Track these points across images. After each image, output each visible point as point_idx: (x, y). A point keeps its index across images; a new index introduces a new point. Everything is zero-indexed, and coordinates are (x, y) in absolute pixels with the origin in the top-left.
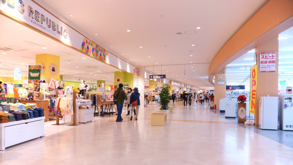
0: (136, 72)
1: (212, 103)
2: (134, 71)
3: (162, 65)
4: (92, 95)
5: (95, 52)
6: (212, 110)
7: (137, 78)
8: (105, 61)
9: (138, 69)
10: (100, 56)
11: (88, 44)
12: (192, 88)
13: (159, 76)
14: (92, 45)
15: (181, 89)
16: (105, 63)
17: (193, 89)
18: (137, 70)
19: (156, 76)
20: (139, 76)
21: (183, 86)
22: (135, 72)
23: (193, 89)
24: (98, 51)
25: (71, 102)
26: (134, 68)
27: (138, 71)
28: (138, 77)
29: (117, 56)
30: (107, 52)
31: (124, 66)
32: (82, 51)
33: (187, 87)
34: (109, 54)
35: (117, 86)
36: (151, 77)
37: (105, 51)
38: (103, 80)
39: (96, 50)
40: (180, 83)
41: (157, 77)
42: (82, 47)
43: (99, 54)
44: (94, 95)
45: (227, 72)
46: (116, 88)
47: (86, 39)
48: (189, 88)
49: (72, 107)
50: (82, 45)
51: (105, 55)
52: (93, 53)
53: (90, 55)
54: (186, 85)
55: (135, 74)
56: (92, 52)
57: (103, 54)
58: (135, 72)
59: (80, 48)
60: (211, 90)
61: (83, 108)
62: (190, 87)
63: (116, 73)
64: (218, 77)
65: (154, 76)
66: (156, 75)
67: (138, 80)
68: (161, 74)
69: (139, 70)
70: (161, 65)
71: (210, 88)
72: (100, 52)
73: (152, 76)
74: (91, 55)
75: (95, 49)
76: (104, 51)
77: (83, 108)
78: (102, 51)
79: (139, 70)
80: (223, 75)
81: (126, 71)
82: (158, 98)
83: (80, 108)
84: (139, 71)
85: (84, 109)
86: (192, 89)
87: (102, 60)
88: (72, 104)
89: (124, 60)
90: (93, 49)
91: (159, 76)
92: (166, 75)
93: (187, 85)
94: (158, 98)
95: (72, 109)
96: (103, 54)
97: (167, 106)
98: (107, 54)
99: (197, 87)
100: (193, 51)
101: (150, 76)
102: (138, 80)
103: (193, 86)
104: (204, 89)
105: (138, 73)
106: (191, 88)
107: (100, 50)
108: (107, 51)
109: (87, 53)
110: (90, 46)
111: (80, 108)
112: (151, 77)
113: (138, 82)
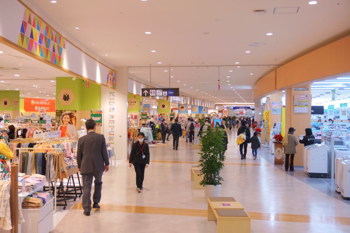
0: (110, 80)
1: (279, 151)
2: (108, 79)
3: (171, 65)
4: (36, 155)
5: (43, 45)
6: (276, 165)
7: (110, 93)
8: (60, 66)
9: (114, 72)
10: (52, 51)
11: (32, 26)
12: (203, 106)
13: (164, 90)
14: (38, 29)
15: (182, 108)
16: (60, 68)
17: (204, 107)
18: (112, 75)
19: (157, 91)
20: (115, 89)
21: (189, 103)
22: (109, 80)
23: (205, 106)
24: (49, 41)
25: (5, 196)
26: (107, 71)
27: (113, 77)
28: (113, 91)
29: (81, 48)
30: (64, 40)
31: (91, 71)
32: (20, 44)
33: (196, 105)
34: (67, 44)
35: (62, 111)
36: (146, 91)
37: (62, 38)
38: (17, 89)
39: (46, 38)
40: (183, 96)
41: (160, 93)
42: (21, 33)
43: (51, 50)
44: (43, 155)
45: (312, 86)
46: (59, 115)
47: (28, 12)
48: (199, 105)
49: (9, 207)
50: (21, 31)
51: (62, 49)
52: (40, 47)
53: (35, 53)
54: (194, 99)
55: (108, 85)
56: (39, 45)
57: (58, 47)
58: (109, 80)
59: (16, 38)
60: (234, 106)
61: (33, 205)
62: (200, 104)
63: (59, 80)
64: (295, 97)
65: (153, 91)
66: (156, 89)
67: (113, 97)
68: (167, 86)
69: (115, 76)
70: (169, 65)
71: (236, 103)
72: (52, 43)
73: (148, 90)
74: (38, 53)
75: (45, 36)
76: (60, 38)
77: (33, 205)
78: (56, 41)
79: (115, 76)
80: (306, 92)
81: (81, 75)
82: (148, 133)
83: (26, 204)
84: (116, 77)
85: (37, 207)
86: (203, 107)
87: (56, 62)
88: (9, 201)
89: (92, 57)
90: (41, 36)
91: (164, 90)
92: (179, 89)
93: (196, 100)
94: (148, 133)
95: (9, 214)
96: (58, 46)
97: (218, 174)
98: (64, 47)
99: (211, 102)
100: (258, 45)
101: (143, 90)
102: (112, 97)
103: (204, 101)
104: (222, 105)
105: (114, 82)
106: (201, 106)
107: (52, 39)
108: (64, 38)
109: (29, 51)
110: (35, 31)
111: (26, 204)
112: (146, 91)
113: (113, 102)
